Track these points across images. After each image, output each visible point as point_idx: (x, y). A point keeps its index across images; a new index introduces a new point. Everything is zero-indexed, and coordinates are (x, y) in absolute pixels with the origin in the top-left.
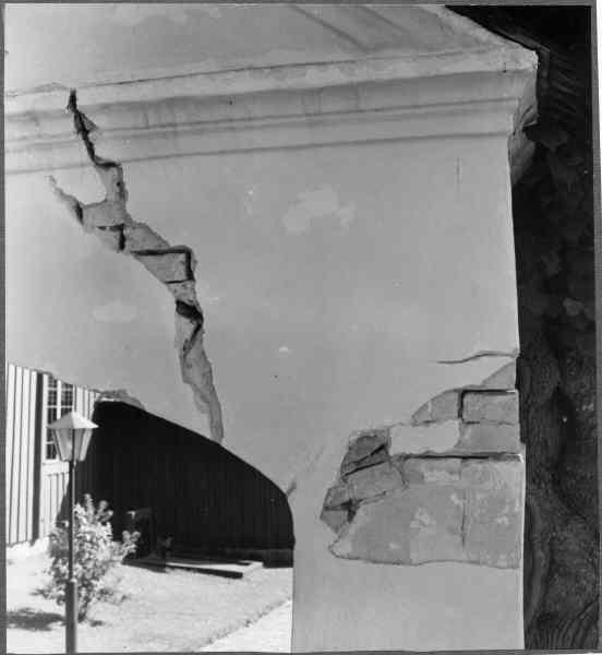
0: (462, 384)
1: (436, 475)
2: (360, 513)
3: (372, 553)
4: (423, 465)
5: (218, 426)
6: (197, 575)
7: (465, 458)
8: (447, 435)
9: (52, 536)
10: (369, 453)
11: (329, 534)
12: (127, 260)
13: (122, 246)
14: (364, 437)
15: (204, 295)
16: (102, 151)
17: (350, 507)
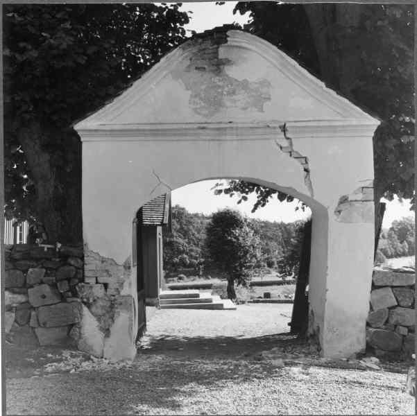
0: (363, 186)
1: (357, 205)
2: (342, 214)
3: (344, 220)
4: (354, 203)
5: (312, 195)
6: (271, 304)
7: (363, 201)
8: (360, 196)
9: (212, 294)
10: (344, 200)
11: (335, 217)
12: (292, 159)
13: (291, 156)
14: (344, 197)
15: (310, 167)
16: (288, 136)
17: (339, 212)
